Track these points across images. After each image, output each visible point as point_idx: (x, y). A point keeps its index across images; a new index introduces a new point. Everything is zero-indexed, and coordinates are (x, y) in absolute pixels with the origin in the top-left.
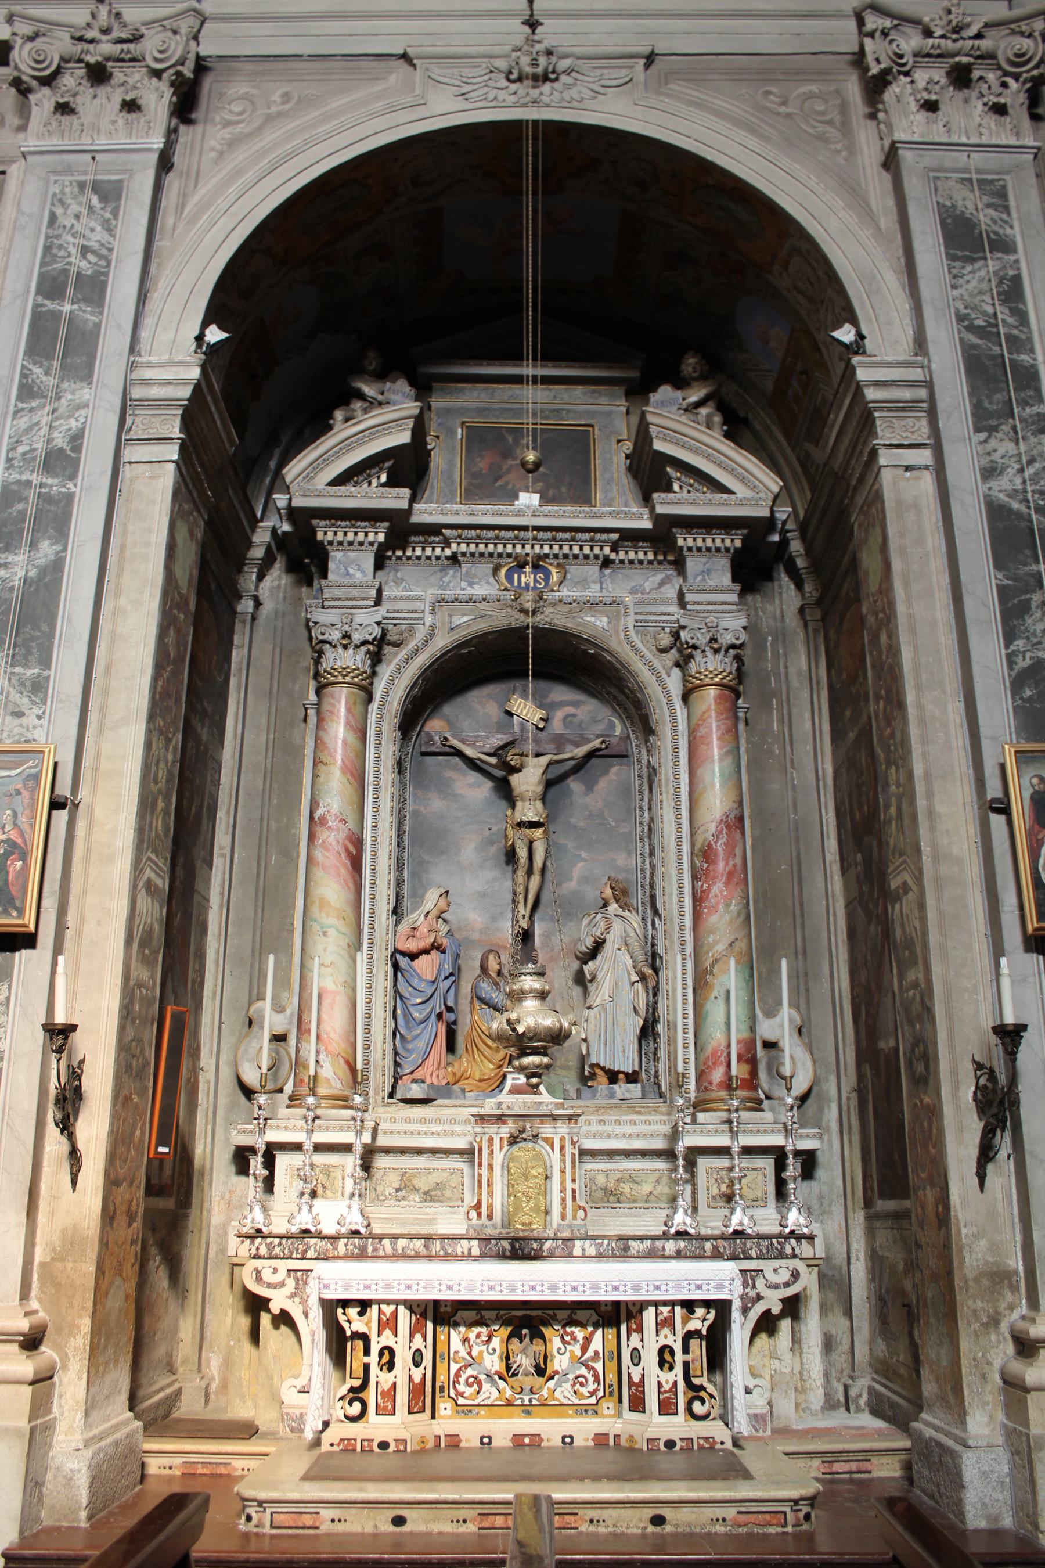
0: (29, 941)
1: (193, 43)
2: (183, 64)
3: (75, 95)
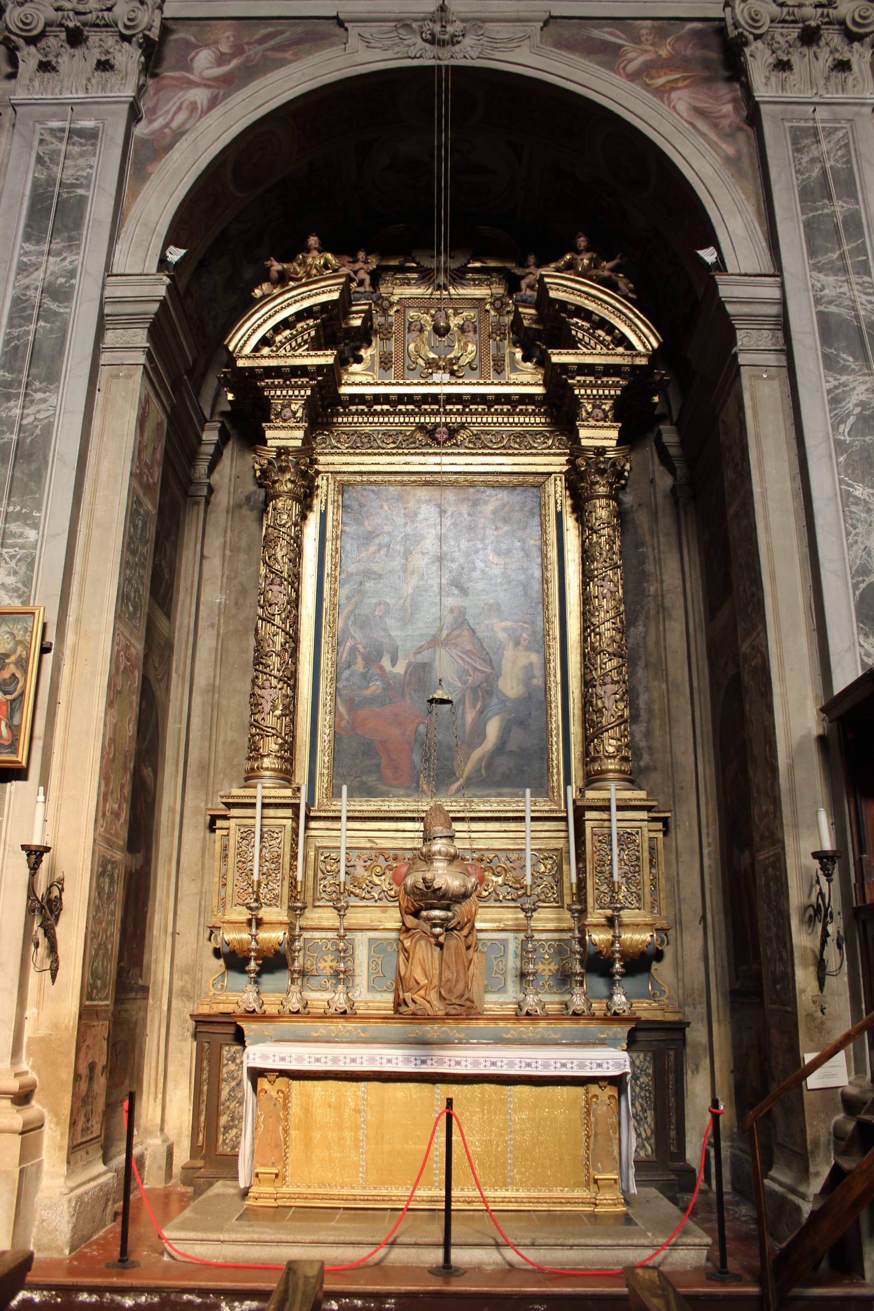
0: (19, 774)
1: (157, 12)
2: (150, 30)
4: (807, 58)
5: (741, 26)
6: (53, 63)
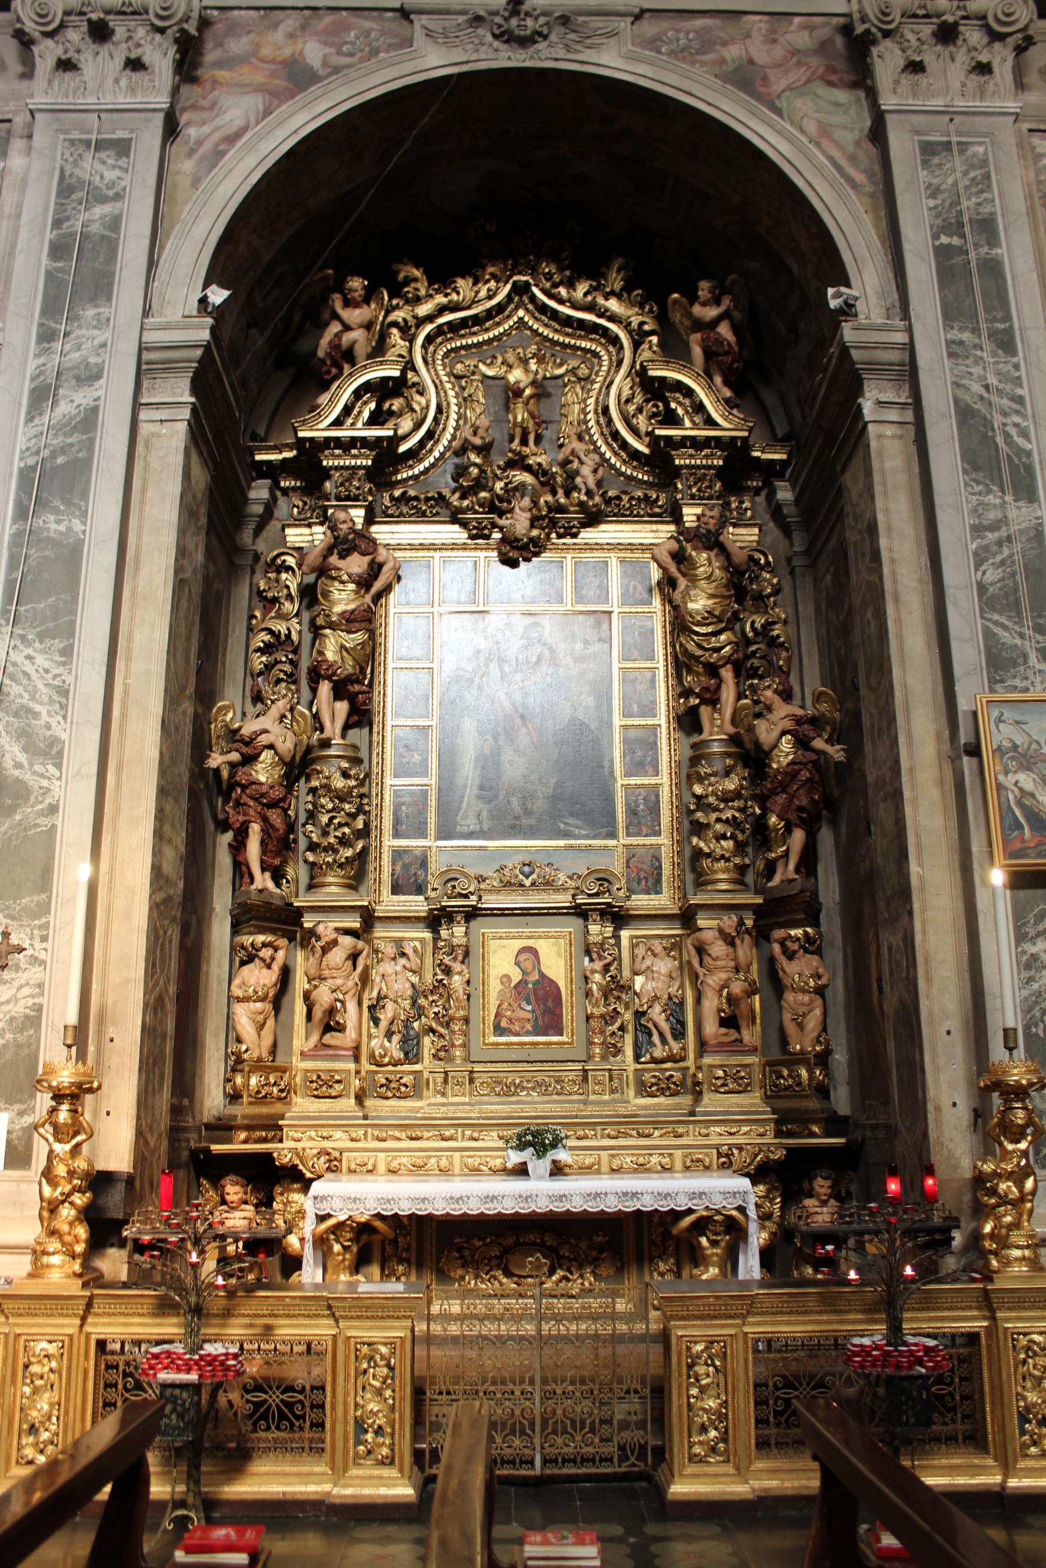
3: (79, 51)
4: (941, 59)
5: (870, 21)
6: (74, 61)
